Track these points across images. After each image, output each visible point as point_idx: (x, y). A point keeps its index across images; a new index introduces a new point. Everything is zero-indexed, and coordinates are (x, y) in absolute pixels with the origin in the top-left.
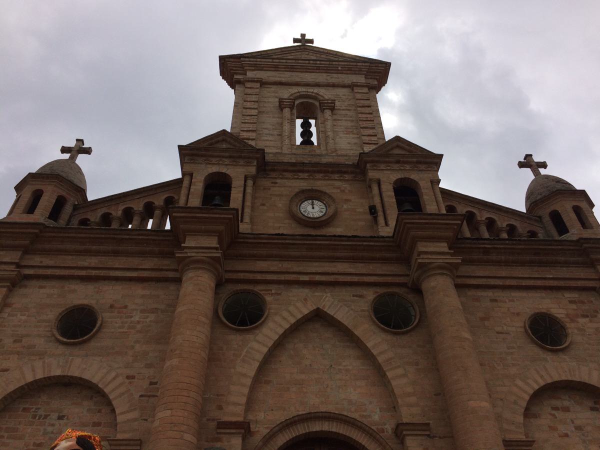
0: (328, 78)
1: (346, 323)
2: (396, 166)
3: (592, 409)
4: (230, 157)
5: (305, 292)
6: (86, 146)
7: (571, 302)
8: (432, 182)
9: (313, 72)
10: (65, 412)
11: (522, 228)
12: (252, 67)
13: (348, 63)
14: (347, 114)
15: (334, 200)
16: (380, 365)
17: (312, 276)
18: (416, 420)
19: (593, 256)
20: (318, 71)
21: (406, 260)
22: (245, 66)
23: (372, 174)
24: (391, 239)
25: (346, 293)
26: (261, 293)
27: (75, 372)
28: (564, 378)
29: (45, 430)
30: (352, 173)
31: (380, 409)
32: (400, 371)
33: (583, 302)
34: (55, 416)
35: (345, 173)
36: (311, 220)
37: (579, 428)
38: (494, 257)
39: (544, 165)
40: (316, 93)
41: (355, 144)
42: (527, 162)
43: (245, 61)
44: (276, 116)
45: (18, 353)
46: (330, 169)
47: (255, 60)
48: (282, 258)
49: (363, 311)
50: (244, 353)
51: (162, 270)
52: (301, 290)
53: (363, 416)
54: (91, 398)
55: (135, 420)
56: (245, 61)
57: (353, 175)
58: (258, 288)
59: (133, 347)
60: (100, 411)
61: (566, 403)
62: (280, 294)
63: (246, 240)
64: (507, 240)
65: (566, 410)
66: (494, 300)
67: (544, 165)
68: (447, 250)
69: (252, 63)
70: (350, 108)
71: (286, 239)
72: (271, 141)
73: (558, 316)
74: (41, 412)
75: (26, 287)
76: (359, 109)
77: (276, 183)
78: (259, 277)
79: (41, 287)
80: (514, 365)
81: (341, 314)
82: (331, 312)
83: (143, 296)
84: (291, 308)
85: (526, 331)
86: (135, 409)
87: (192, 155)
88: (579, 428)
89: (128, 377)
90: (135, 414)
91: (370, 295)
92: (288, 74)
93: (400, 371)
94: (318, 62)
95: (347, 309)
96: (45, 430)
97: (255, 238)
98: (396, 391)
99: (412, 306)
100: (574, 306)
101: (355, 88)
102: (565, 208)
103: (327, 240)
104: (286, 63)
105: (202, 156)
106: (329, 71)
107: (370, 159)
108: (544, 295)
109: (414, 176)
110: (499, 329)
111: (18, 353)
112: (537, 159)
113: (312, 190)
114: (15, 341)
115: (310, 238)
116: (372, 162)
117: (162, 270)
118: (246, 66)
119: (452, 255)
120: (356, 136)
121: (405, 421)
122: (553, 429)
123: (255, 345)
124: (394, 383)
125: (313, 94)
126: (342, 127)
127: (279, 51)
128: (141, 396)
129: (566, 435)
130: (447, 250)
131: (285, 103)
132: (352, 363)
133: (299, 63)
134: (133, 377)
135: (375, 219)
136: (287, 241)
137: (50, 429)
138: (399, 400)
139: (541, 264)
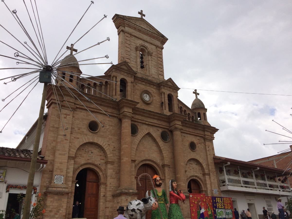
0: (150, 39)
1: (155, 137)
2: (169, 89)
3: (196, 165)
4: (127, 73)
5: (146, 127)
6: (262, 213)
7: (198, 139)
8: (176, 97)
9: (146, 35)
10: (93, 151)
11: (188, 112)
12: (127, 25)
13: (157, 36)
14: (154, 59)
15: (152, 96)
16: (161, 149)
17: (149, 123)
18: (167, 164)
19: (205, 129)
20: (147, 35)
21: (169, 122)
22: (125, 24)
23: (163, 90)
24: (168, 116)
25: (155, 129)
26: (137, 125)
27: (95, 141)
28: (194, 158)
29: (89, 156)
30: (156, 86)
31: (159, 160)
32: (165, 152)
33: (200, 140)
34: (90, 152)
35: (155, 85)
36: (144, 100)
37: (193, 168)
38: (187, 125)
39: (198, 94)
40: (147, 46)
41: (156, 73)
42: (195, 93)
43: (125, 22)
44: (134, 52)
45: (80, 133)
46: (151, 83)
47: (129, 22)
48: (142, 116)
49: (159, 135)
50: (134, 142)
51: (113, 113)
52: (145, 126)
53: (156, 161)
54: (98, 148)
55: (112, 156)
56: (125, 22)
57: (156, 87)
58: (136, 123)
59: (108, 136)
60: (101, 152)
61: (192, 163)
62: (141, 126)
63: (135, 109)
64: (191, 122)
65: (192, 164)
66: (184, 136)
67: (144, 16)
68: (181, 124)
69: (128, 23)
70: (155, 56)
71: (145, 111)
72: (133, 64)
73: (195, 143)
74: (87, 150)
75: (76, 111)
76: (159, 58)
77: (137, 84)
78: (137, 120)
79: (81, 112)
80: (186, 153)
81: (154, 135)
82: (152, 134)
83: (108, 121)
84: (143, 131)
85: (189, 146)
86: (111, 154)
87: (117, 69)
88: (193, 168)
89: (108, 145)
90: (111, 155)
91: (161, 130)
92: (138, 33)
93: (165, 152)
94: (148, 32)
95: (155, 133)
96: (89, 156)
97: (137, 109)
98: (164, 156)
99: (169, 135)
100: (198, 141)
101: (158, 48)
102: (202, 112)
103: (154, 113)
104: (139, 28)
105: (119, 70)
106: (151, 37)
107: (163, 85)
108: (193, 137)
109: (172, 94)
110: (184, 144)
111: (80, 133)
112: (144, 13)
113: (147, 91)
114: (78, 129)
115: (151, 112)
116: (163, 85)
117: (113, 113)
118: (126, 24)
119: (182, 126)
120: (156, 69)
121: (165, 164)
122: (189, 168)
123: (136, 140)
124: (164, 155)
125: (146, 46)
126: (153, 64)
127: (135, 18)
128: (112, 150)
129: (191, 170)
130: (181, 124)
131: (138, 49)
132: (155, 148)
133: (142, 29)
134: (110, 145)
135: (162, 106)
136: (145, 112)
137: (90, 155)
138: (165, 159)
139: (195, 129)
